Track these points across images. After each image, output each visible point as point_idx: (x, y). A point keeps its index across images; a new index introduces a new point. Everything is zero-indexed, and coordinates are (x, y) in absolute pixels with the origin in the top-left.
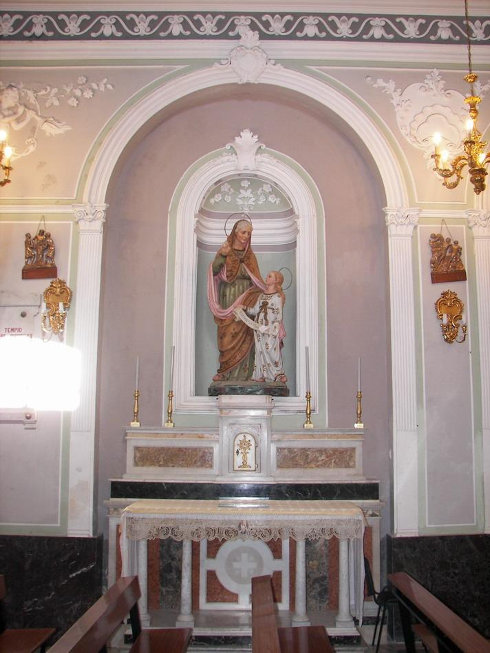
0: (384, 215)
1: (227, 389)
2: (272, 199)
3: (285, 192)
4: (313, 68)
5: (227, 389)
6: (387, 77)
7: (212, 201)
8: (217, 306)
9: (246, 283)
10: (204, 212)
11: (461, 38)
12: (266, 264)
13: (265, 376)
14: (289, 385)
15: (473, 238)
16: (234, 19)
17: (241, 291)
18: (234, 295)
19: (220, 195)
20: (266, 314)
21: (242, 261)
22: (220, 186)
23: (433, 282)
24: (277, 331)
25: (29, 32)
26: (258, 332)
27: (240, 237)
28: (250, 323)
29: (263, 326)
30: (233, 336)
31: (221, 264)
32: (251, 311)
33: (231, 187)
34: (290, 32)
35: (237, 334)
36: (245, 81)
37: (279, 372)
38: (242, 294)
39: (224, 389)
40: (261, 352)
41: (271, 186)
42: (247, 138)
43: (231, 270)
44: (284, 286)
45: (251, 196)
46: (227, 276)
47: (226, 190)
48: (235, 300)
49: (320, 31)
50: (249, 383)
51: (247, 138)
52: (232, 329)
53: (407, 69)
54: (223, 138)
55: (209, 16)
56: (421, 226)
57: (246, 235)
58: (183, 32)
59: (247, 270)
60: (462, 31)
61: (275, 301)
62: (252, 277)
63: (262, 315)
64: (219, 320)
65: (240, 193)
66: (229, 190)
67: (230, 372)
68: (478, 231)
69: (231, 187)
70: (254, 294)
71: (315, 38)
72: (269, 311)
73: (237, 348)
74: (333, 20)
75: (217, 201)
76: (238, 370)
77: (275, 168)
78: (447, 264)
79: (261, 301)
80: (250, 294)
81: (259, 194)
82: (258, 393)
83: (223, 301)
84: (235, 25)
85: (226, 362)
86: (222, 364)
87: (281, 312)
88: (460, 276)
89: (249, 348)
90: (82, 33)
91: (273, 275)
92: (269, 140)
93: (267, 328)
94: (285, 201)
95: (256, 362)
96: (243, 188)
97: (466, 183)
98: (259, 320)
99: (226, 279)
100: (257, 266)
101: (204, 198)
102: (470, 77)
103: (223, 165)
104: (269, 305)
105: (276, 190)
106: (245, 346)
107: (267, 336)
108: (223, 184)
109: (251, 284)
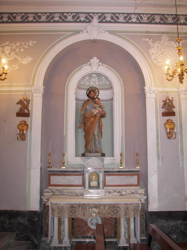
0: (144, 90)
4: (120, 34)
6: (150, 37)
11: (11, 21)
15: (180, 99)
16: (131, 16)
23: (163, 116)
25: (27, 20)
34: (48, 20)
36: (93, 39)
42: (95, 60)
49: (137, 20)
51: (95, 60)
53: (174, 35)
54: (87, 60)
55: (96, 14)
56: (31, 94)
58: (111, 20)
60: (176, 20)
68: (182, 96)
71: (136, 23)
74: (142, 16)
78: (168, 109)
84: (80, 17)
88: (173, 114)
90: (149, 21)
92: (102, 61)
94: (110, 83)
97: (177, 79)
101: (110, 81)
102: (178, 38)
105: (106, 78)
108: (86, 77)
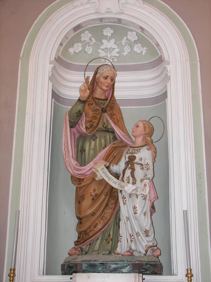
1: (84, 266)
2: (137, 49)
3: (153, 38)
5: (84, 266)
7: (71, 50)
8: (74, 162)
9: (109, 136)
10: (61, 61)
12: (131, 117)
13: (133, 247)
14: (162, 259)
17: (103, 145)
18: (95, 149)
19: (80, 45)
20: (133, 170)
21: (104, 111)
22: (80, 33)
24: (147, 189)
26: (123, 192)
27: (101, 82)
28: (113, 182)
29: (130, 185)
30: (93, 199)
31: (79, 111)
32: (115, 168)
33: (92, 37)
35: (97, 196)
37: (151, 244)
38: (104, 148)
39: (81, 265)
40: (128, 218)
41: (137, 34)
43: (91, 121)
44: (154, 138)
45: (116, 47)
46: (86, 128)
47: (87, 39)
48: (95, 155)
50: (112, 257)
52: (92, 190)
57: (109, 80)
59: (110, 121)
61: (144, 155)
62: (116, 129)
63: (128, 172)
64: (77, 180)
65: (103, 44)
66: (90, 39)
67: (90, 244)
69: (92, 37)
70: (117, 150)
72: (137, 168)
73: (98, 214)
75: (77, 51)
76: (99, 241)
77: (139, 10)
79: (127, 156)
80: (114, 149)
81: (124, 44)
82: (124, 270)
83: (81, 156)
85: (85, 231)
86: (80, 233)
87: (151, 168)
89: (112, 214)
91: (141, 125)
93: (134, 187)
95: (123, 231)
96: (106, 37)
98: (125, 178)
99: (84, 131)
100: (122, 118)
101: (61, 44)
103: (82, 8)
104: (137, 160)
105: (144, 38)
106: (108, 212)
107: (134, 197)
108: (83, 32)
109: (115, 138)
